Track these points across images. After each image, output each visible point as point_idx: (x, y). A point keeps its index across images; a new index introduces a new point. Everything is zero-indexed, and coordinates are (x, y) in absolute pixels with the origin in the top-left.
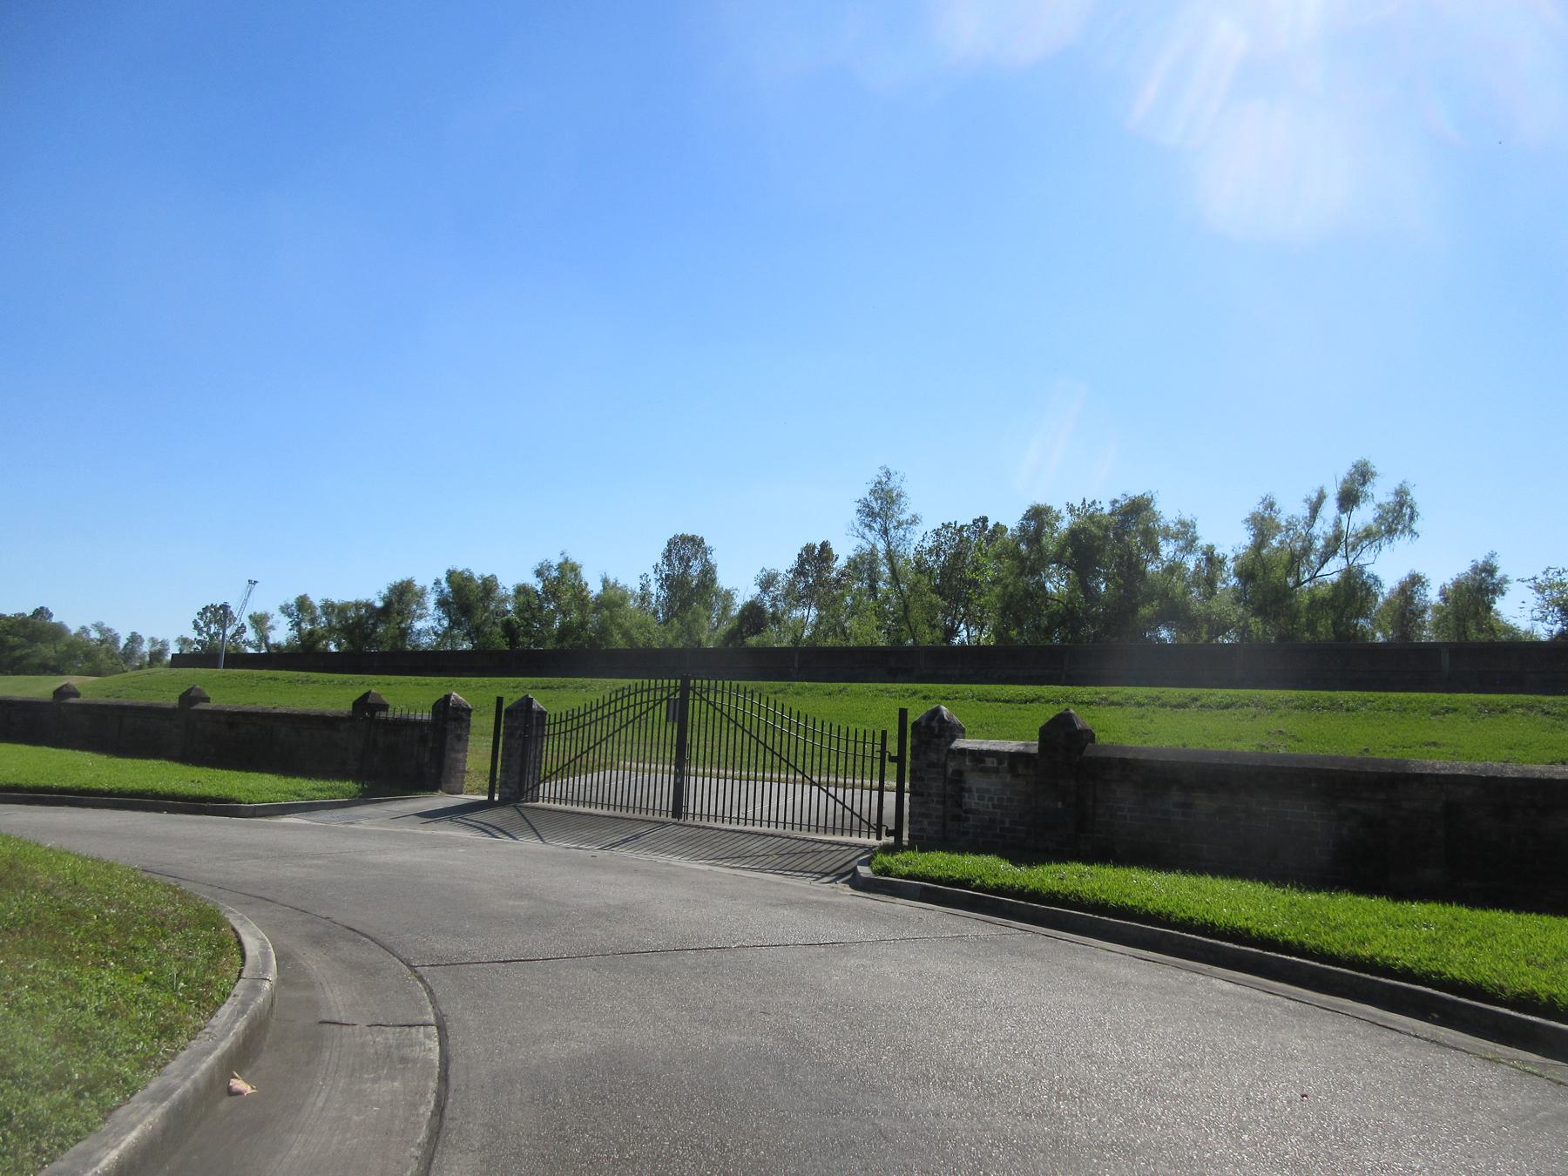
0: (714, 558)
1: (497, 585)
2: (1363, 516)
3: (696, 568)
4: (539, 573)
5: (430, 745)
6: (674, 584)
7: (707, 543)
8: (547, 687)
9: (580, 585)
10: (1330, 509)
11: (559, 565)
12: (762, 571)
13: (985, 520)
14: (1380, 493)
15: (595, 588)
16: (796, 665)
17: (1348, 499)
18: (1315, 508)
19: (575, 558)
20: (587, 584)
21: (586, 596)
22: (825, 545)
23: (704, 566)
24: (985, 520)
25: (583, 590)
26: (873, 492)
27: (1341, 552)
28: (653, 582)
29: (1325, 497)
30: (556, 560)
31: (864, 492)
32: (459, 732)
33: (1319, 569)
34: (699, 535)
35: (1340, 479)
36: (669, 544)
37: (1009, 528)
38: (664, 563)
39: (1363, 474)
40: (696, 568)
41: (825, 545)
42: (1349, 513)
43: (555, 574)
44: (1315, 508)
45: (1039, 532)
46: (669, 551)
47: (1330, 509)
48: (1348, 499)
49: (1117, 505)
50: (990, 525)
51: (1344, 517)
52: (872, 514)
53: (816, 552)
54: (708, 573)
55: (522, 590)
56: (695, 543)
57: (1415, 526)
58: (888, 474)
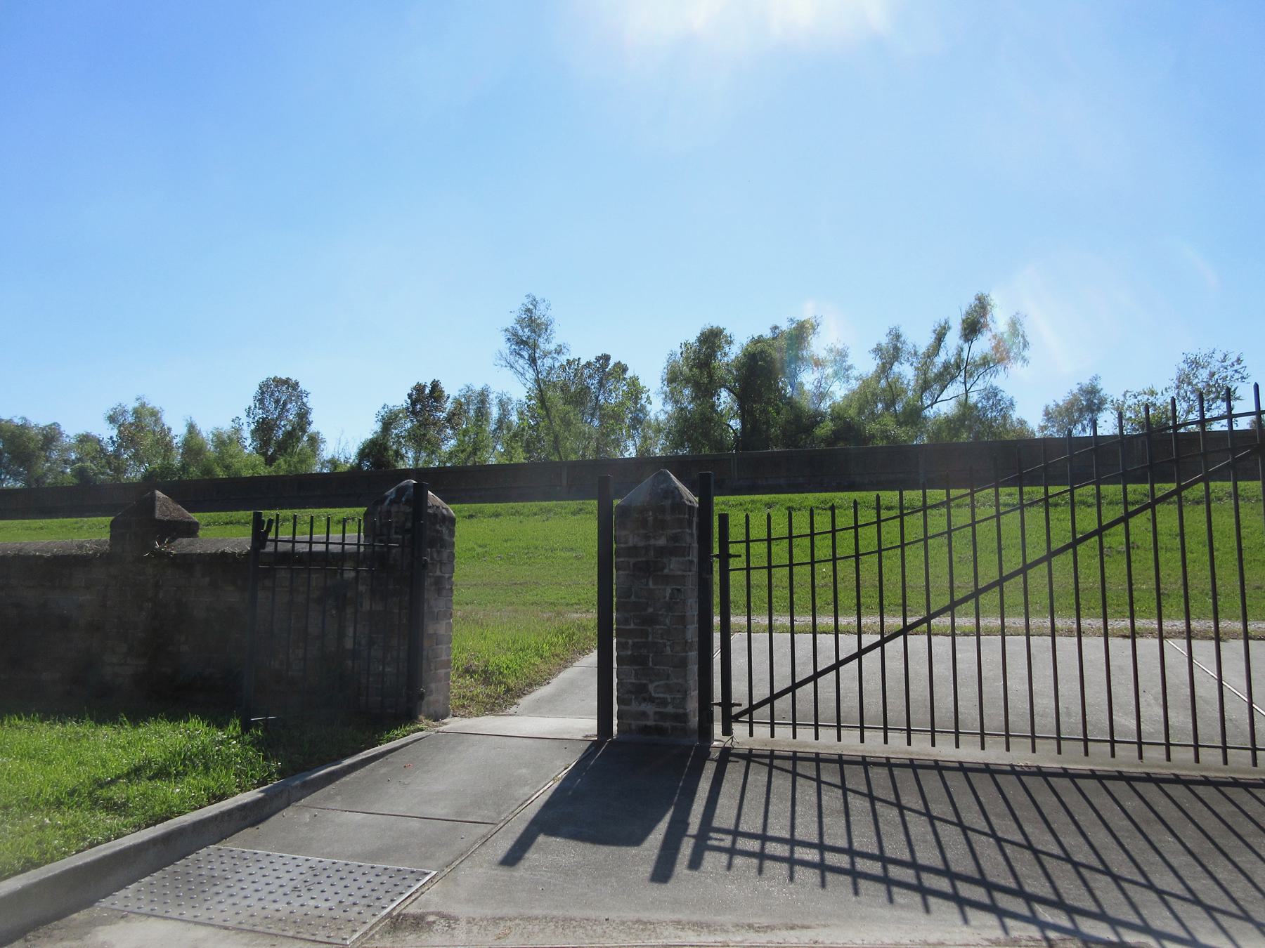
0: (311, 402)
1: (61, 434)
2: (982, 346)
3: (293, 408)
4: (112, 419)
5: (366, 606)
6: (264, 429)
7: (302, 386)
8: (231, 523)
9: (163, 430)
10: (953, 339)
11: (134, 409)
12: (384, 408)
13: (606, 358)
14: (999, 321)
15: (178, 432)
16: (564, 482)
17: (972, 328)
18: (940, 337)
19: (153, 402)
20: (169, 429)
21: (171, 441)
22: (435, 385)
23: (301, 409)
24: (606, 358)
25: (166, 435)
26: (520, 321)
27: (960, 379)
28: (245, 427)
29: (949, 328)
30: (131, 405)
31: (510, 322)
32: (438, 573)
33: (939, 396)
34: (294, 378)
35: (964, 312)
36: (261, 388)
37: (514, 399)
38: (255, 406)
39: (982, 306)
40: (293, 408)
41: (435, 385)
42: (970, 342)
43: (131, 419)
44: (940, 337)
45: (711, 355)
46: (263, 393)
47: (953, 339)
48: (972, 328)
49: (777, 331)
50: (612, 363)
51: (966, 346)
52: (521, 342)
53: (427, 391)
54: (303, 415)
55: (85, 439)
56: (289, 385)
57: (1026, 353)
58: (535, 302)
